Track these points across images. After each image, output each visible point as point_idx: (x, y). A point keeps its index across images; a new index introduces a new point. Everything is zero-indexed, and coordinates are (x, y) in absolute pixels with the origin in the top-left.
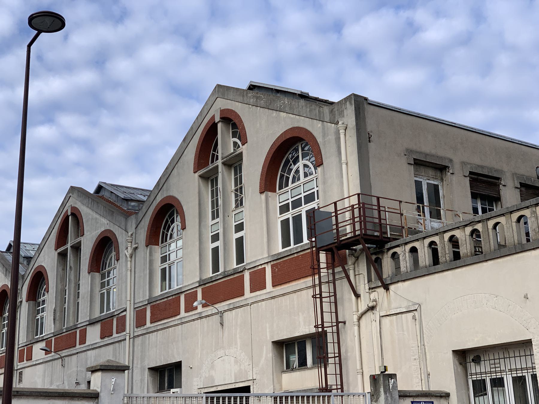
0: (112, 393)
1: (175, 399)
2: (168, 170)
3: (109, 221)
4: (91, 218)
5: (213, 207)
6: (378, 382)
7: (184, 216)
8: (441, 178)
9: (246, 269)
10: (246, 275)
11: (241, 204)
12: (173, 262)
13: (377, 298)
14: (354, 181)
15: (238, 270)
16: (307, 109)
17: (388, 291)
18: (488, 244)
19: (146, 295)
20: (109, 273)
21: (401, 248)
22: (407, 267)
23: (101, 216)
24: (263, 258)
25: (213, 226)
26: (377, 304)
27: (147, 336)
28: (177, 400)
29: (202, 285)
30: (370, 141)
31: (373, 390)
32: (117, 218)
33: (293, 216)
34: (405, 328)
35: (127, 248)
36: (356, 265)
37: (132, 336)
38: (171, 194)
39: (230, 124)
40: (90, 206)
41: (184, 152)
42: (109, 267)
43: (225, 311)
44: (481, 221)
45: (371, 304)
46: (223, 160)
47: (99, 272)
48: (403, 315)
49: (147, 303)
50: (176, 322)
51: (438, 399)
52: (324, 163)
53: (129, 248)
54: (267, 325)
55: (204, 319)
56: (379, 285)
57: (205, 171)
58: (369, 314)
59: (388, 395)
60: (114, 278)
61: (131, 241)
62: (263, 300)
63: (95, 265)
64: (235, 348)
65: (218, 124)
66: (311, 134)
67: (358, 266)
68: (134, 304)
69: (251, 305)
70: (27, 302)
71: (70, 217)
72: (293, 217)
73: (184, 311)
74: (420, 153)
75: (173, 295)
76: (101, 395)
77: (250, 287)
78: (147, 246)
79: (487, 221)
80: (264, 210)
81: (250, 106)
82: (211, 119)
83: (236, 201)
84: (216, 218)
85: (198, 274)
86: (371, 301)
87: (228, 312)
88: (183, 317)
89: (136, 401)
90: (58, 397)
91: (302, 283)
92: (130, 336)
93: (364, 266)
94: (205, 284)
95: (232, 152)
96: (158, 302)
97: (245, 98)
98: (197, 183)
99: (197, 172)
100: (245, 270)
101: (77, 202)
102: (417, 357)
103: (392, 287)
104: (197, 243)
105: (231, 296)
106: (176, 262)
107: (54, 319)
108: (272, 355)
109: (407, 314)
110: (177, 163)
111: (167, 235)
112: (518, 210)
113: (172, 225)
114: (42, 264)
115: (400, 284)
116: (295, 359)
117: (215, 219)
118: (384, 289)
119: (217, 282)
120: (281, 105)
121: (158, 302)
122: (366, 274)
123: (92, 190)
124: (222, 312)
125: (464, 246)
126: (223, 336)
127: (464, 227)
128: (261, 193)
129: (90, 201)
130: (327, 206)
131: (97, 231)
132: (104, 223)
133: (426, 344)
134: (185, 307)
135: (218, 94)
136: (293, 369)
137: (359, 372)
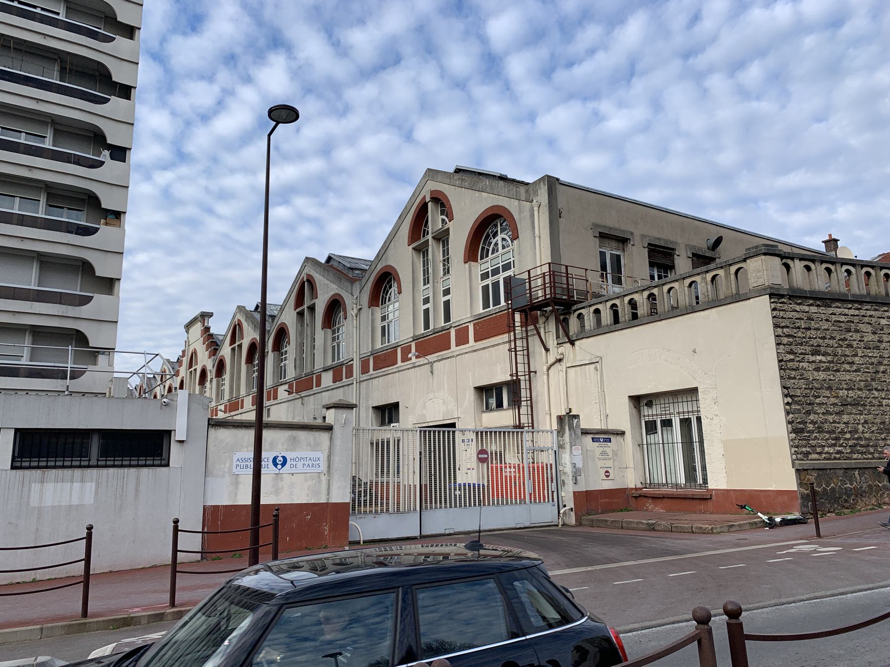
11: (448, 272)
30: (560, 217)
35: (353, 309)
37: (358, 381)
38: (389, 264)
43: (435, 362)
45: (558, 357)
51: (615, 436)
58: (557, 365)
62: (466, 353)
67: (548, 324)
71: (306, 283)
75: (391, 348)
78: (369, 307)
83: (444, 269)
94: (418, 339)
101: (312, 270)
102: (597, 401)
103: (577, 343)
104: (411, 305)
112: (690, 276)
115: (584, 340)
116: (493, 402)
123: (323, 260)
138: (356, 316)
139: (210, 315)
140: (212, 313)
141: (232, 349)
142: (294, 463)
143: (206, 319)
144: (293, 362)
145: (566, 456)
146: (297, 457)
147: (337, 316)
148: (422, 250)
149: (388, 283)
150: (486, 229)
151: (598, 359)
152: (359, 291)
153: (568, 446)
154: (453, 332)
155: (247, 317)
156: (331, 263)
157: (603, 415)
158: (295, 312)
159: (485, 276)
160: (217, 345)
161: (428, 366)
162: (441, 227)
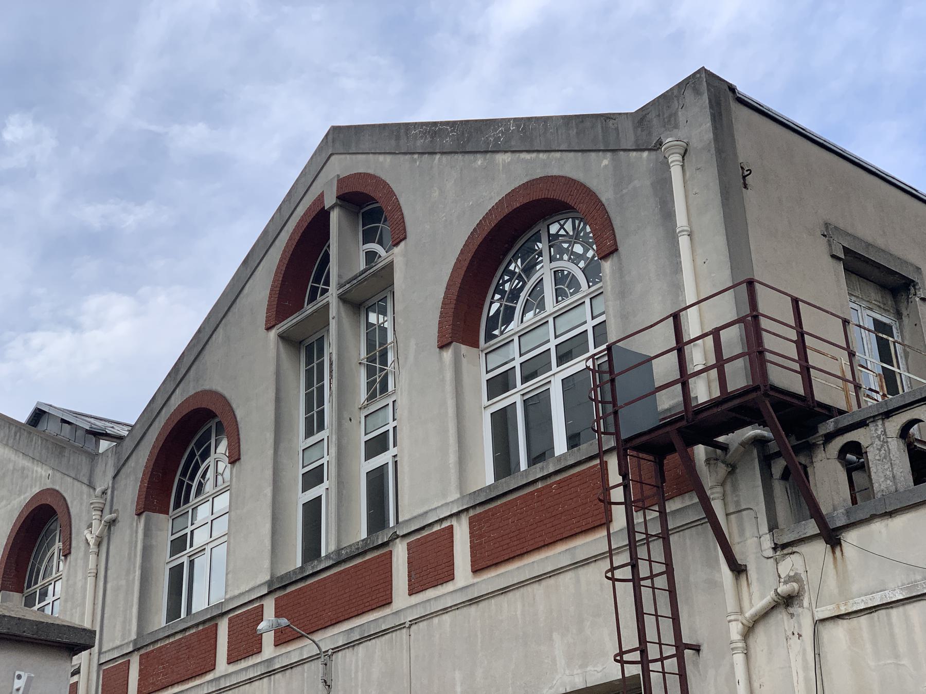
2: (201, 335)
5: (309, 408)
7: (238, 431)
8: (895, 311)
9: (398, 537)
10: (398, 551)
11: (384, 387)
12: (203, 548)
13: (801, 570)
14: (713, 275)
15: (377, 541)
16: (570, 132)
19: (130, 631)
20: (44, 594)
21: (873, 428)
23: (35, 462)
25: (307, 453)
29: (276, 590)
30: (745, 186)
32: (72, 459)
34: (902, 648)
36: (728, 487)
39: (358, 214)
40: (11, 441)
43: (337, 650)
45: (783, 589)
46: (341, 291)
47: (20, 590)
48: (895, 612)
49: (131, 649)
50: (203, 690)
53: (95, 523)
54: (458, 675)
56: (808, 535)
57: (294, 321)
60: (55, 603)
61: (101, 506)
62: (445, 610)
63: (13, 574)
66: (583, 186)
67: (735, 488)
68: (99, 655)
69: (409, 627)
72: (524, 401)
73: (225, 660)
74: (855, 238)
75: (197, 625)
77: (409, 581)
78: (139, 515)
80: (449, 387)
82: (314, 203)
83: (370, 385)
84: (318, 432)
85: (267, 564)
86: (782, 580)
87: (347, 650)
88: (222, 676)
94: (284, 587)
95: (362, 269)
96: (159, 645)
97: (403, 141)
99: (273, 326)
100: (396, 539)
103: (851, 538)
104: (268, 491)
105: (354, 609)
106: (208, 548)
110: (224, 317)
115: (878, 527)
117: (314, 435)
118: (827, 544)
119: (316, 580)
120: (499, 138)
121: (159, 645)
124: (330, 653)
128: (443, 346)
130: (652, 326)
131: (22, 497)
134: (228, 651)
135: (333, 146)
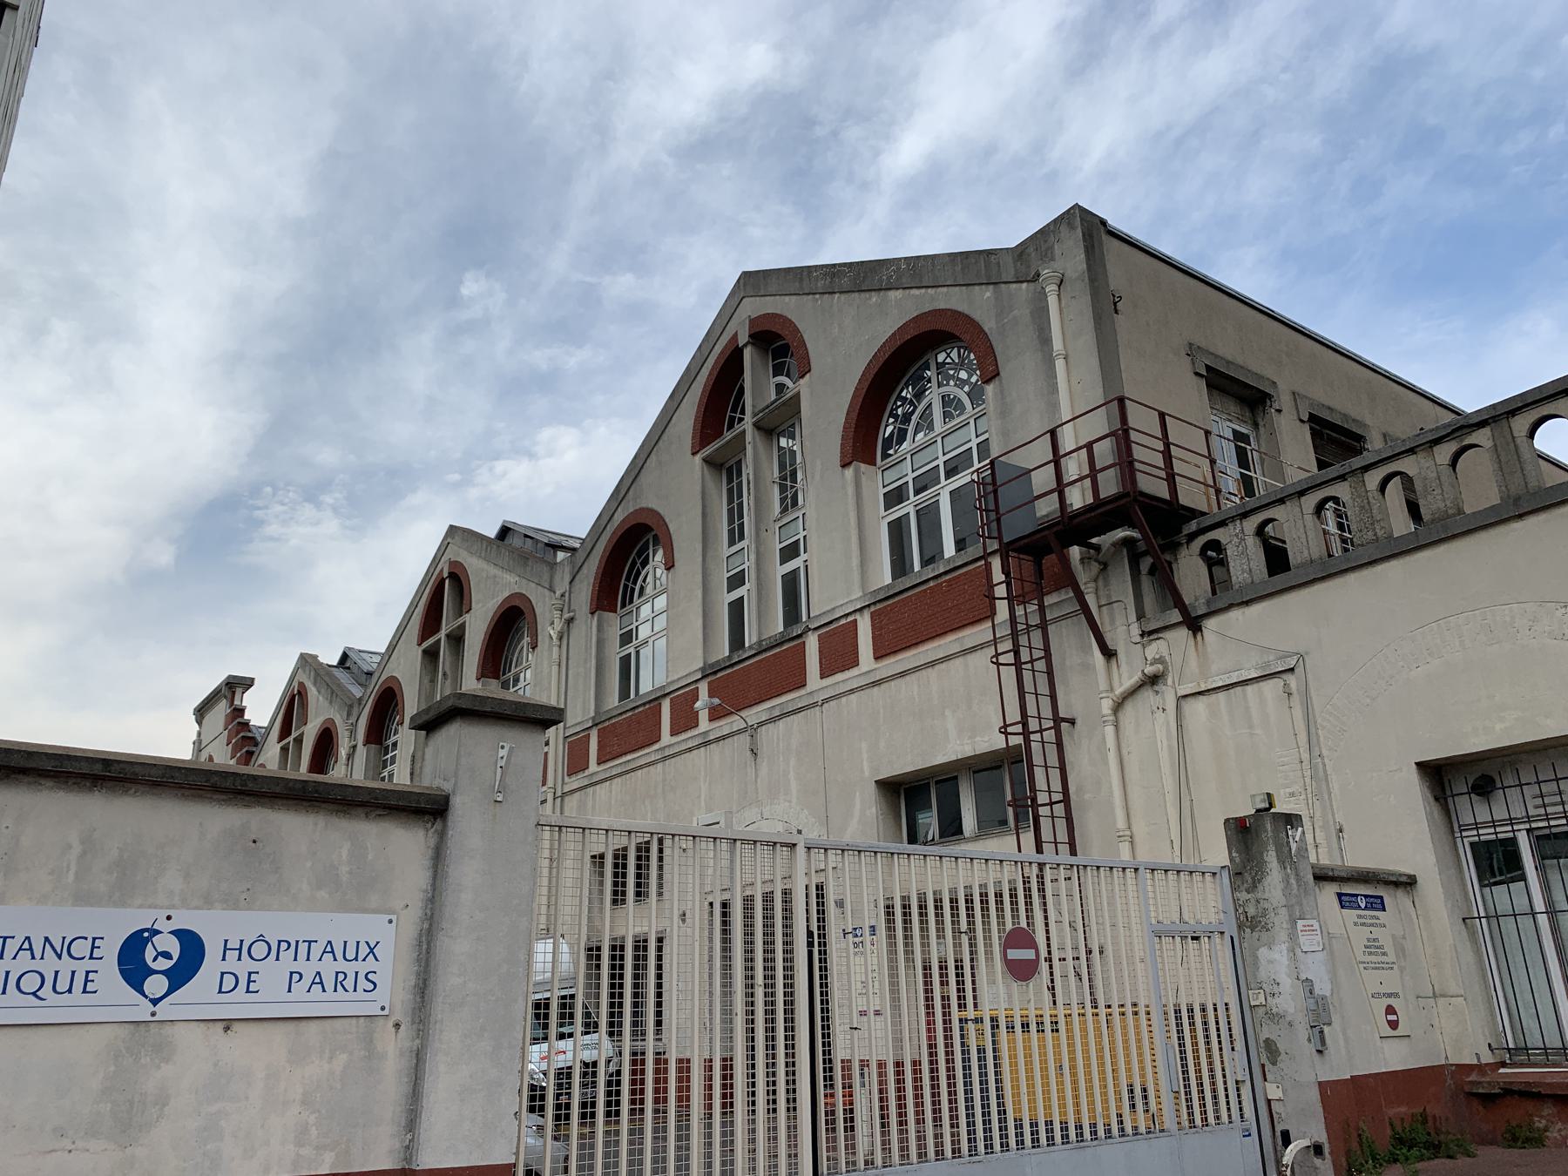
0: (499, 799)
1: (711, 845)
2: (637, 461)
3: (519, 576)
4: (485, 576)
5: (731, 521)
6: (1257, 836)
9: (810, 629)
11: (795, 503)
13: (1165, 654)
16: (956, 268)
17: (1199, 637)
18: (1519, 474)
19: (589, 709)
22: (1250, 570)
24: (851, 601)
26: (1166, 668)
27: (590, 790)
28: (718, 847)
29: (708, 675)
30: (1116, 312)
31: (1238, 860)
33: (917, 508)
35: (553, 623)
36: (1101, 583)
37: (559, 793)
38: (644, 505)
41: (671, 418)
42: (516, 667)
43: (761, 724)
44: (1490, 421)
45: (1149, 670)
46: (755, 419)
47: (497, 677)
48: (1249, 689)
49: (590, 724)
51: (1391, 889)
52: (1001, 373)
54: (864, 745)
55: (714, 745)
58: (1147, 694)
59: (1289, 871)
61: (561, 606)
62: (852, 691)
64: (785, 800)
65: (745, 351)
67: (1106, 584)
70: (364, 745)
71: (447, 581)
75: (644, 704)
76: (457, 802)
78: (592, 613)
79: (1508, 418)
81: (817, 296)
82: (730, 341)
83: (783, 500)
85: (700, 652)
86: (1148, 662)
87: (769, 725)
89: (584, 844)
90: (285, 802)
91: (950, 642)
92: (555, 793)
93: (1124, 581)
94: (715, 673)
95: (773, 399)
98: (700, 474)
101: (461, 550)
102: (1296, 788)
103: (1210, 625)
104: (699, 593)
107: (412, 774)
108: (877, 812)
109: (1261, 684)
111: (633, 590)
113: (643, 568)
114: (394, 675)
115: (1235, 614)
116: (930, 821)
117: (735, 544)
122: (1130, 600)
123: (492, 532)
125: (1435, 493)
126: (756, 777)
127: (1431, 447)
128: (844, 465)
129: (484, 546)
131: (495, 600)
132: (510, 582)
133: (1325, 753)
136: (927, 842)
137: (1124, 836)
138: (560, 639)
139: (247, 683)
140: (252, 680)
141: (282, 748)
142: (243, 968)
143: (239, 691)
144: (409, 763)
145: (1277, 956)
146: (261, 938)
147: (516, 646)
148: (726, 467)
149: (639, 554)
150: (887, 402)
151: (1292, 662)
152: (567, 578)
153: (1280, 921)
154: (812, 644)
155: (317, 674)
156: (509, 540)
157: (1325, 827)
158: (420, 652)
159: (895, 497)
160: (256, 744)
161: (744, 739)
162: (773, 397)
